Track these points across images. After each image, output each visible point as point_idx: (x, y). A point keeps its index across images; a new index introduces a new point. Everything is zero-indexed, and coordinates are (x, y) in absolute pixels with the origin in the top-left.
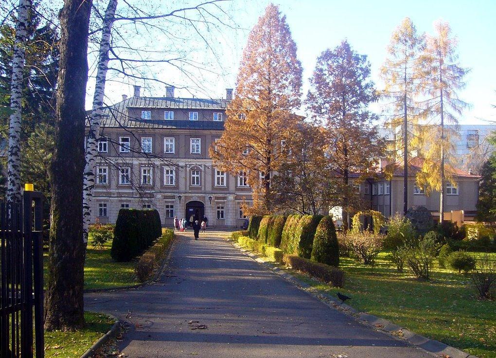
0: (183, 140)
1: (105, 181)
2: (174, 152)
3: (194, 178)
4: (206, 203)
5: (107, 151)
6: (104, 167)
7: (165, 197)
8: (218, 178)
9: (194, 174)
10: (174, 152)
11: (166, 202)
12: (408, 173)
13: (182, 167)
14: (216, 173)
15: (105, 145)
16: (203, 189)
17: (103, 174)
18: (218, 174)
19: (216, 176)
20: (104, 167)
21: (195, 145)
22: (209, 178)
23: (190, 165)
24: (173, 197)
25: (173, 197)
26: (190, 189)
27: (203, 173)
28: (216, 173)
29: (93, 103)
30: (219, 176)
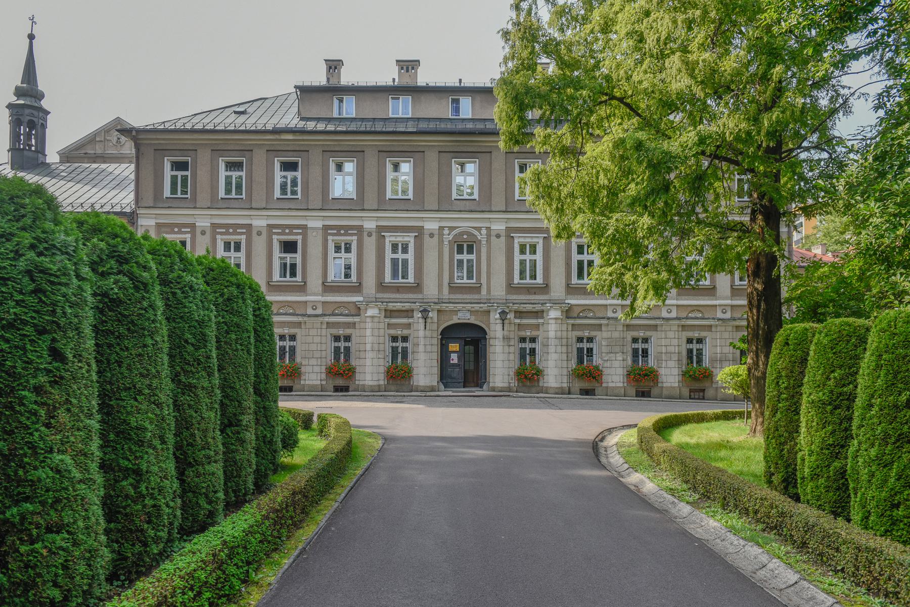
0: (435, 164)
1: (534, 277)
2: (411, 196)
3: (460, 262)
4: (492, 327)
5: (244, 196)
6: (237, 237)
7: (389, 313)
8: (523, 262)
9: (460, 251)
10: (411, 196)
11: (390, 326)
12: (146, 238)
13: (431, 235)
14: (388, 247)
15: (185, 179)
16: (484, 291)
17: (400, 256)
18: (523, 252)
19: (517, 257)
20: (237, 237)
21: (466, 179)
22: (499, 261)
23: (451, 229)
24: (408, 313)
25: (408, 313)
26: (453, 288)
27: (484, 250)
28: (388, 247)
29: (17, 88)
30: (523, 257)
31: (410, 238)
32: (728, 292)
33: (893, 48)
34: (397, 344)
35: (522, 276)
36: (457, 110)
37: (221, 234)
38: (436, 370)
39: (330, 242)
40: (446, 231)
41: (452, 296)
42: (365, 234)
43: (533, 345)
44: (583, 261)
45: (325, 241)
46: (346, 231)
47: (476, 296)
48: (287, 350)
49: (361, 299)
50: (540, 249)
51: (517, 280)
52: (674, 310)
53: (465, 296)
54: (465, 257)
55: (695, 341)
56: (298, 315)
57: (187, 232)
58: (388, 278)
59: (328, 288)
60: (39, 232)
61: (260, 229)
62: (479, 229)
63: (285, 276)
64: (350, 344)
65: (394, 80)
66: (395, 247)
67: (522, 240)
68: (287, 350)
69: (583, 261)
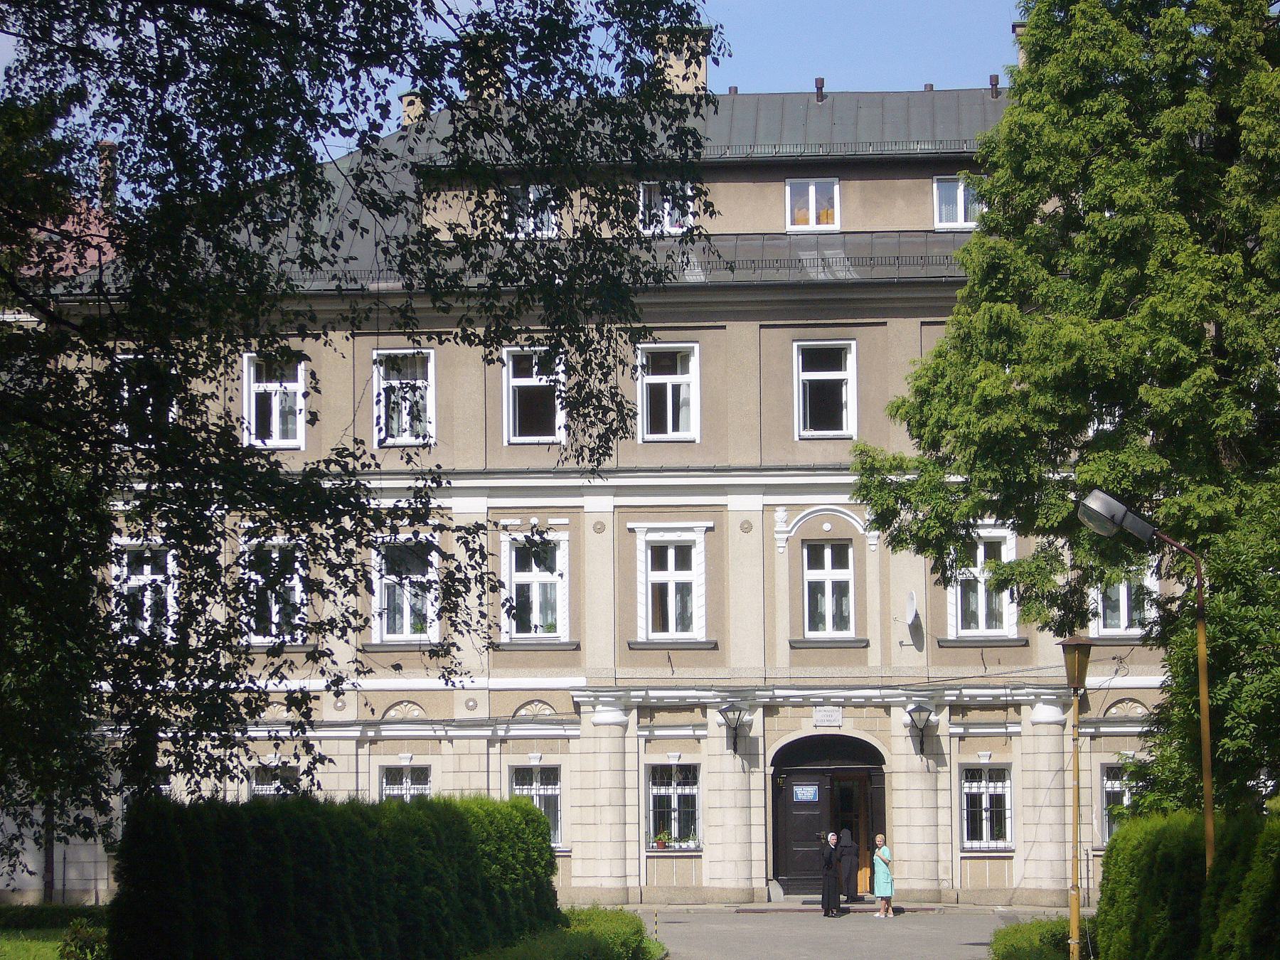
1: (685, 622)
3: (816, 589)
9: (816, 562)
14: (643, 557)
33: (151, 105)
34: (680, 791)
38: (760, 851)
40: (780, 514)
41: (798, 672)
43: (998, 788)
47: (857, 671)
48: (675, 804)
49: (581, 681)
50: (698, 556)
52: (482, 698)
53: (830, 671)
54: (828, 575)
55: (985, 775)
56: (432, 722)
58: (644, 631)
60: (470, 538)
61: (746, 517)
63: (664, 628)
64: (694, 790)
66: (658, 556)
68: (675, 804)
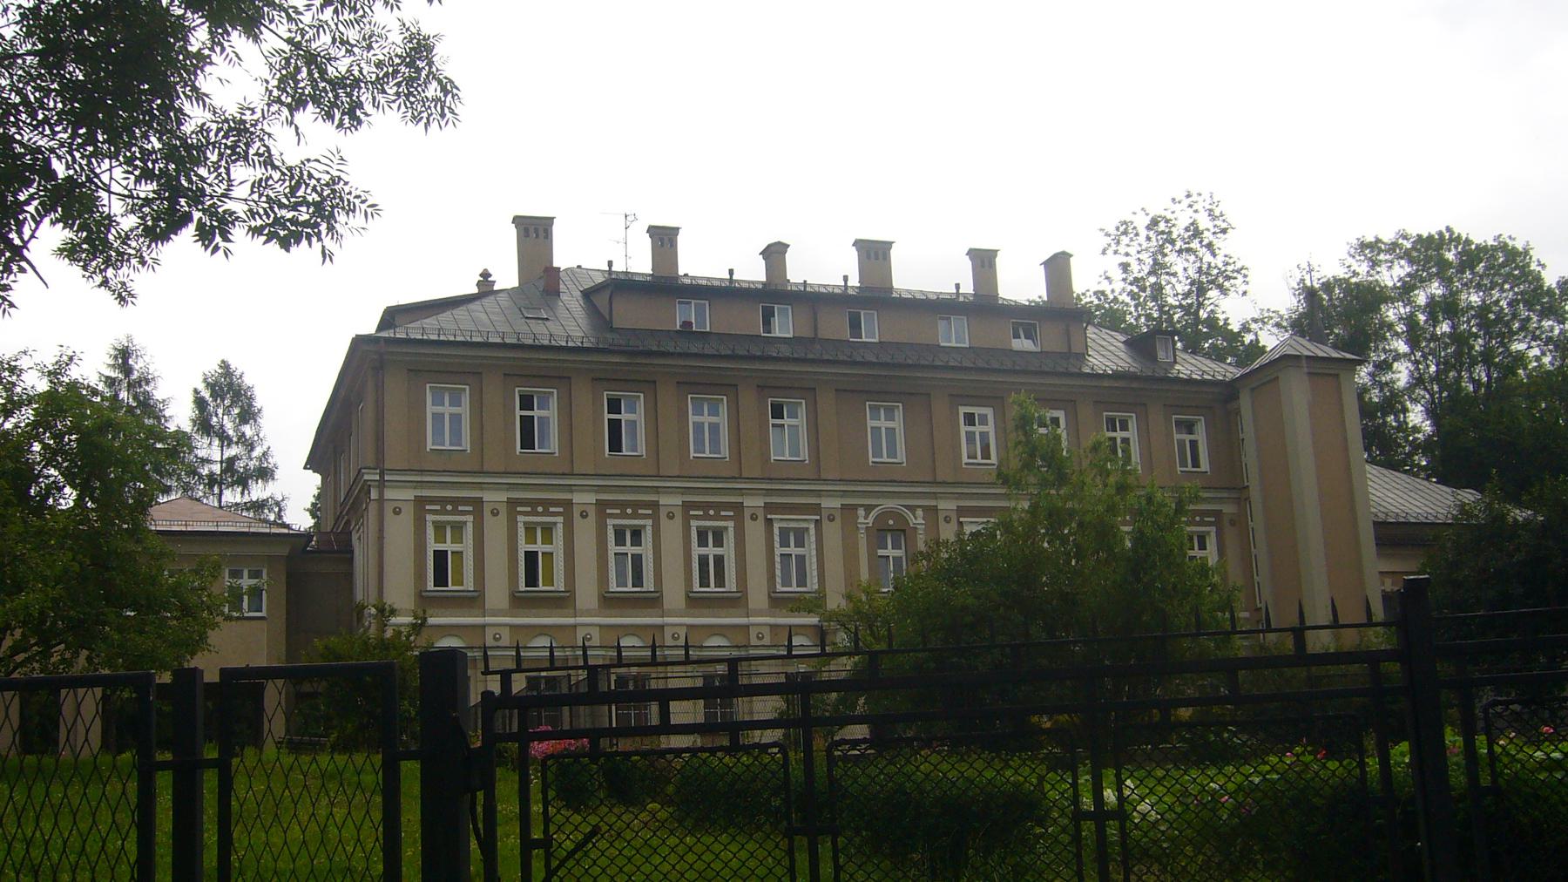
1: (720, 581)
23: (869, 508)
28: (430, 531)
31: (807, 522)
32: (504, 603)
35: (704, 582)
36: (767, 323)
37: (697, 517)
39: (520, 525)
42: (576, 515)
44: (707, 557)
45: (687, 528)
46: (443, 507)
51: (697, 587)
57: (468, 513)
59: (610, 602)
62: (912, 509)
65: (846, 278)
67: (784, 525)
69: (707, 557)
